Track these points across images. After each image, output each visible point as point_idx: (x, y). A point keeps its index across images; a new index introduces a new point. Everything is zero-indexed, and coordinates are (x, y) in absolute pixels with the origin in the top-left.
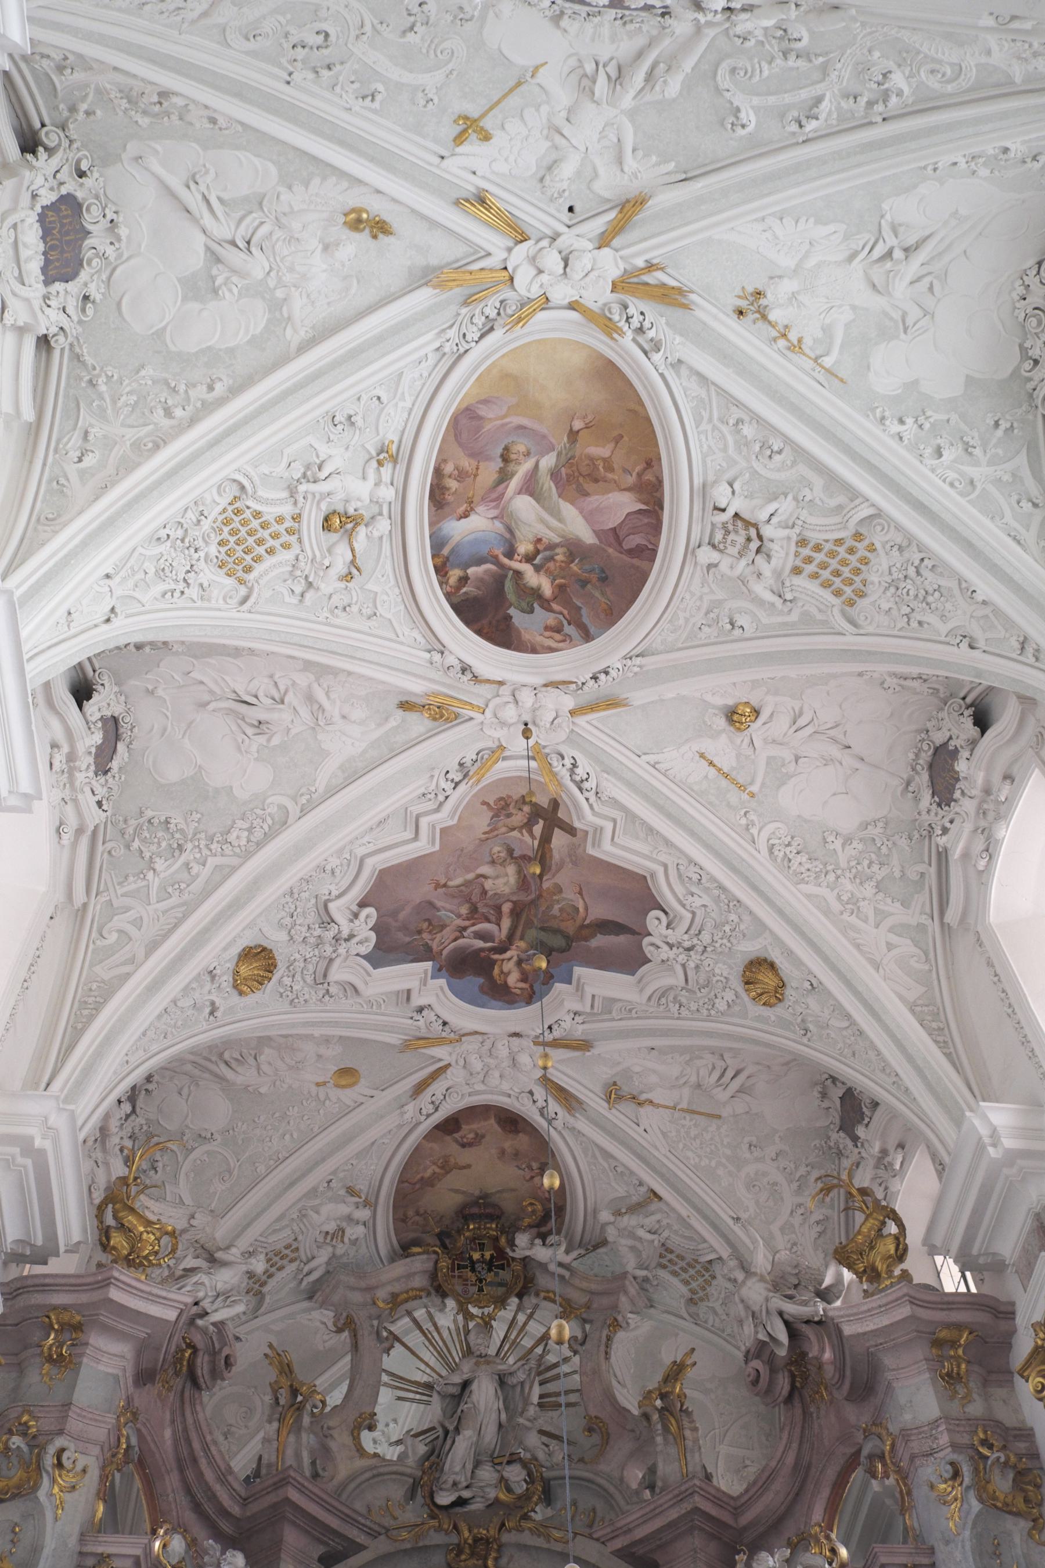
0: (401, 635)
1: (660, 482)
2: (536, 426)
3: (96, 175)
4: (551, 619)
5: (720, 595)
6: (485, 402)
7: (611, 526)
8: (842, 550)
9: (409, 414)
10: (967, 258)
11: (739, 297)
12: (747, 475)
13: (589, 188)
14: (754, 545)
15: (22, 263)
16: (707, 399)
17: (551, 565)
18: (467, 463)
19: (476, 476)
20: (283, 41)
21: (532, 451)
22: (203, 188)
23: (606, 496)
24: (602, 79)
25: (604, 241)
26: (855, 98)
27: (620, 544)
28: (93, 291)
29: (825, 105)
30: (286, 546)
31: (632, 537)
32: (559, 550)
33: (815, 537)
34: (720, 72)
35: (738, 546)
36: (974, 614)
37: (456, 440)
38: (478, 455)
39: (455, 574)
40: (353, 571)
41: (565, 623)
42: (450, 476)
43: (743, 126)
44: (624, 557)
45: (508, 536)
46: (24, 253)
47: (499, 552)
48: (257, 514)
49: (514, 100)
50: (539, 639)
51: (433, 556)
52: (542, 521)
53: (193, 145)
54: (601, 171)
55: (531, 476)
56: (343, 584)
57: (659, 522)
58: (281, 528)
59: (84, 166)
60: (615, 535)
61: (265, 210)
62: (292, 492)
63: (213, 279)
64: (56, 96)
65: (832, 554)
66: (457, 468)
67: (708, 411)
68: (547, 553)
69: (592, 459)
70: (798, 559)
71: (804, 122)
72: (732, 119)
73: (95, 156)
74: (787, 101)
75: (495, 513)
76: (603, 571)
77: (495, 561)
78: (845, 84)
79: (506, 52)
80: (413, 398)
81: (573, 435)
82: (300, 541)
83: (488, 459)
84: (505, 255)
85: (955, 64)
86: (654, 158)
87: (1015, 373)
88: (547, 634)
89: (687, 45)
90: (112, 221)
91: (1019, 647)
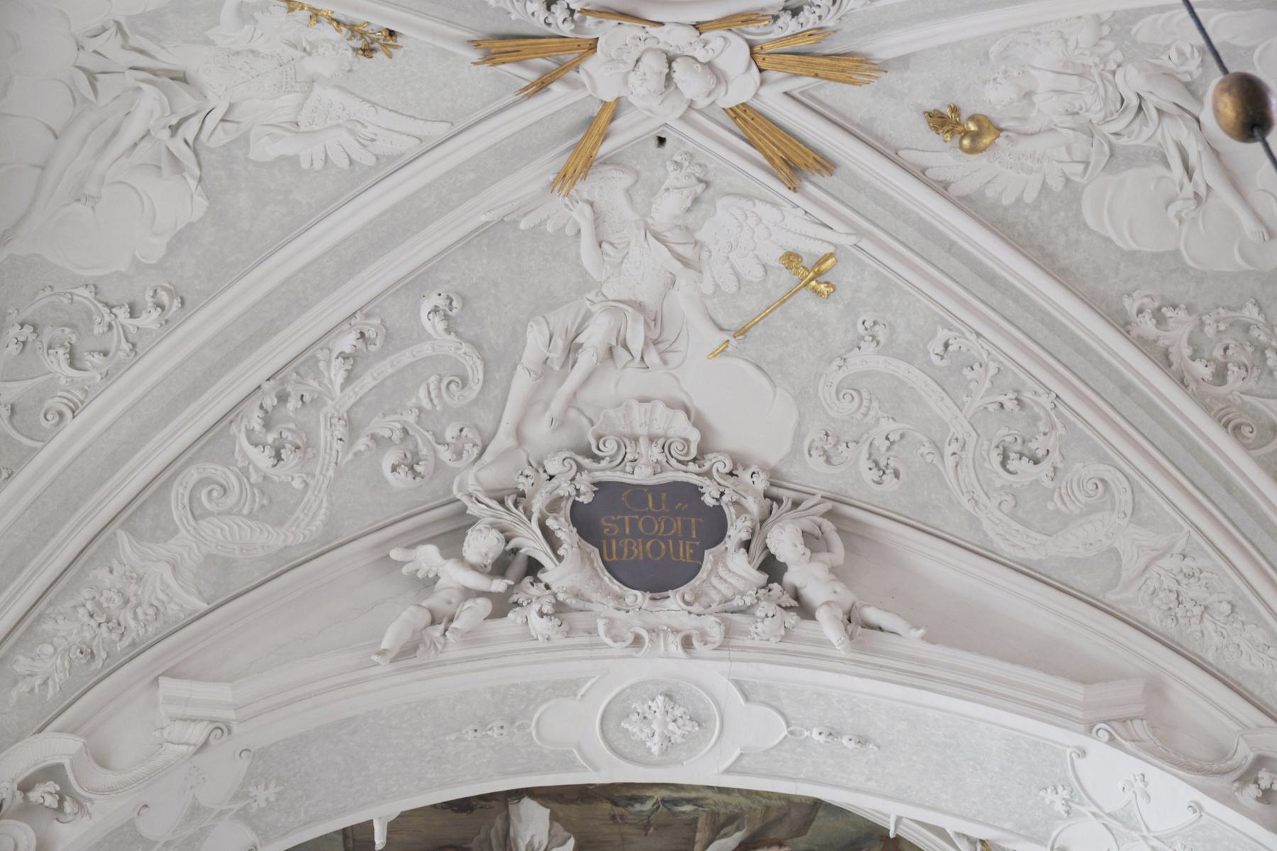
10: (51, 129)
13: (637, 173)
20: (1059, 465)
22: (1189, 188)
25: (614, 110)
29: (339, 378)
34: (481, 376)
43: (436, 310)
53: (1190, 263)
54: (621, 200)
71: (360, 344)
79: (764, 381)
84: (764, 91)
85: (203, 517)
86: (549, 228)
89: (530, 404)
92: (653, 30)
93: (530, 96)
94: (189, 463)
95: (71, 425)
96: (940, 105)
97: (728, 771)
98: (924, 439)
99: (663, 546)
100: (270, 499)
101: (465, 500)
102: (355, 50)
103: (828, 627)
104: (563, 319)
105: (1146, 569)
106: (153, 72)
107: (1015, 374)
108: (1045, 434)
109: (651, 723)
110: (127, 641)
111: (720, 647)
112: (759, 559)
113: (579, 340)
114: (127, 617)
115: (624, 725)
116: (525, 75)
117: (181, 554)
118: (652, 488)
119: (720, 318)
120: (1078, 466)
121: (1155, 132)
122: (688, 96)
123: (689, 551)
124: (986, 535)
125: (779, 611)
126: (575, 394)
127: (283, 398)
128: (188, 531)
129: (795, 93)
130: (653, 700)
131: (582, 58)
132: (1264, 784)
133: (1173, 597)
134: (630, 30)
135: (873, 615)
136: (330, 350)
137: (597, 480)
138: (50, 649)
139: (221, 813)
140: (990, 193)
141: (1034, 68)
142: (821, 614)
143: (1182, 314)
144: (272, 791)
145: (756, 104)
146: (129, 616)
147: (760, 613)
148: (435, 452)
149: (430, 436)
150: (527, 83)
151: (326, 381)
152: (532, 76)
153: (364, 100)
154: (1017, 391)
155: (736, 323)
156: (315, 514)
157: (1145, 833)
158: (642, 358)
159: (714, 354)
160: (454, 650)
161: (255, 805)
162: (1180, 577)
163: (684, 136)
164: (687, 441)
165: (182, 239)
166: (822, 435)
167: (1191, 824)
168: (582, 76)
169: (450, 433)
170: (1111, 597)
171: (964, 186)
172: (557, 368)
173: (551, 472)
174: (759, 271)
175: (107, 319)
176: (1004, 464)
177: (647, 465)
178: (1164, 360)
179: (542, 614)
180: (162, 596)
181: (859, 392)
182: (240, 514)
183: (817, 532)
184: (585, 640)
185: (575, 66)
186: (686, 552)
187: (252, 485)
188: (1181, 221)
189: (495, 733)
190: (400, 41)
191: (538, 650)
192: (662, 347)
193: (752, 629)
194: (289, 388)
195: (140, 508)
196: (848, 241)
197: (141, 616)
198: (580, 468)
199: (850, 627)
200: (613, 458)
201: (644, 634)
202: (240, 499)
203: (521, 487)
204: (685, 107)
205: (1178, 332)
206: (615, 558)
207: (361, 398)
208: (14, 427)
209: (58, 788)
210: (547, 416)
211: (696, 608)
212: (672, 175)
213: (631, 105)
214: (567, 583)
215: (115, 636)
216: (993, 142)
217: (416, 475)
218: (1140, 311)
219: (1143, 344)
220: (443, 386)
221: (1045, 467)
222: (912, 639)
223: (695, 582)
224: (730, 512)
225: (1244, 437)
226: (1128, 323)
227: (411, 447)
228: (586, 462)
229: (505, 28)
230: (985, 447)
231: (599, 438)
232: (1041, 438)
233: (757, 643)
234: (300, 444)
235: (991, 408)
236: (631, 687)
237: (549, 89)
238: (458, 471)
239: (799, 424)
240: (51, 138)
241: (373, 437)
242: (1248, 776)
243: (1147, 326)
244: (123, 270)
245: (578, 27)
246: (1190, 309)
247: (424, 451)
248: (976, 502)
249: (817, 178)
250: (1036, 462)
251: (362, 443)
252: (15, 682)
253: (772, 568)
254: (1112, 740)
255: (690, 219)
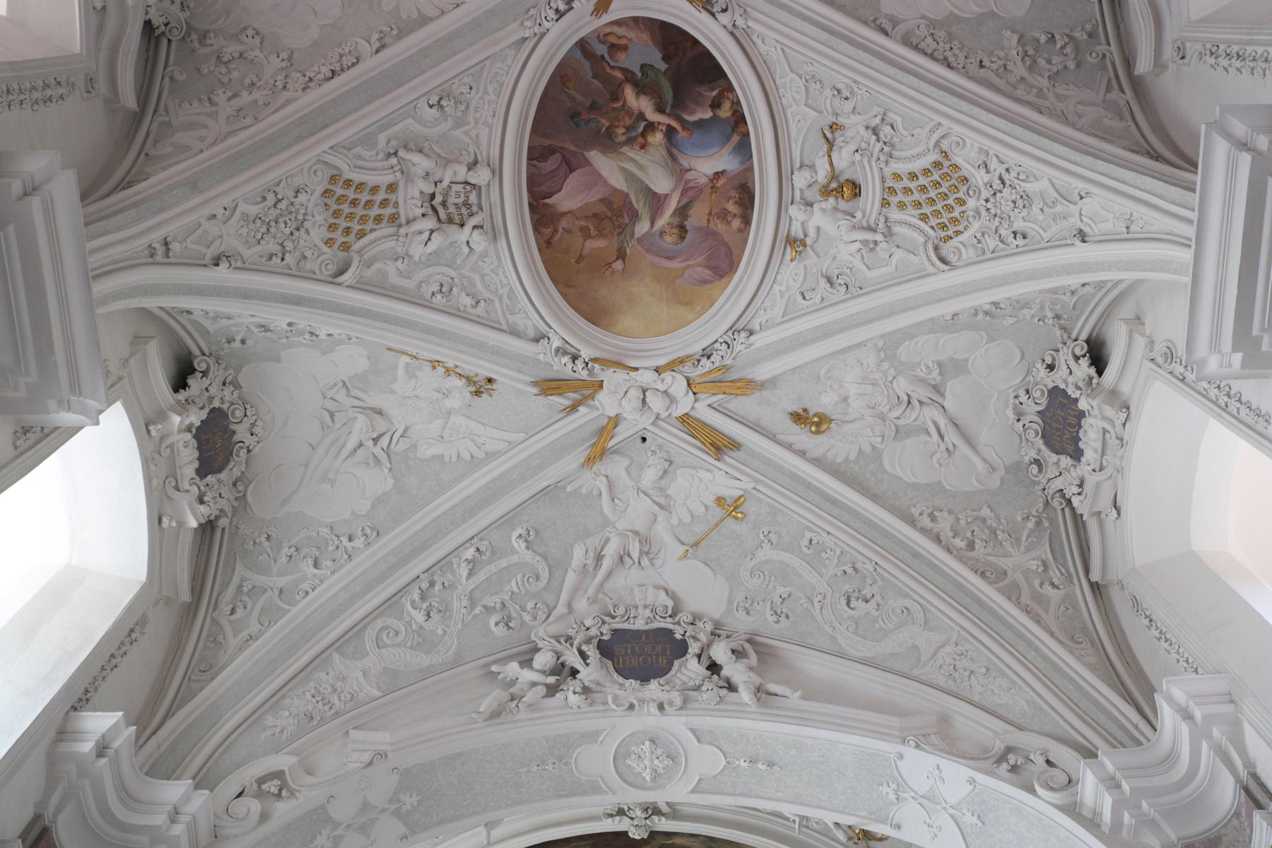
0: (779, 49)
1: (536, 229)
2: (656, 259)
3: (1027, 459)
4: (623, 59)
5: (458, 133)
6: (705, 282)
7: (575, 173)
8: (356, 227)
9: (775, 278)
10: (311, 445)
11: (493, 390)
12: (458, 262)
13: (632, 458)
14: (439, 199)
15: (1101, 439)
16: (507, 314)
17: (628, 122)
18: (719, 226)
19: (710, 214)
20: (881, 602)
21: (657, 238)
22: (943, 447)
23: (584, 202)
24: (635, 554)
25: (616, 421)
26: (444, 587)
27: (564, 156)
28: (1042, 372)
29: (464, 572)
30: (897, 177)
31: (555, 167)
32: (622, 139)
33: (385, 230)
34: (547, 574)
35: (452, 193)
36: (220, 240)
37: (730, 249)
38: (709, 234)
39: (725, 112)
40: (831, 135)
41: (607, 57)
42: (735, 215)
44: (556, 143)
45: (674, 151)
46: (1098, 445)
47: (682, 134)
48: (924, 218)
49: (700, 529)
50: (632, 35)
51: (747, 134)
52: (641, 167)
53: (949, 488)
54: (623, 474)
55: (656, 213)
56: (841, 120)
57: (530, 191)
58: (900, 197)
59: (1035, 469)
60: (571, 164)
61: (893, 428)
62: (889, 234)
63: (941, 373)
64: (1051, 534)
65: (363, 219)
66: (729, 223)
67: (504, 303)
68: (633, 134)
69: (601, 235)
70: (394, 200)
71: (477, 555)
72: (531, 538)
73: (1025, 472)
74: (493, 566)
75: (689, 176)
76: (577, 125)
77: (683, 122)
78: (455, 595)
79: (709, 571)
80: (772, 292)
81: (621, 255)
82: (883, 180)
83: (699, 229)
84: (697, 405)
85: (383, 647)
86: (584, 491)
87: (238, 369)
88: (623, 42)
89: (576, 589)
90: (1018, 420)
91: (171, 247)
92: (633, 374)
93: (569, 414)
94: (377, 617)
95: (312, 595)
96: (796, 408)
97: (693, 791)
98: (802, 596)
99: (650, 659)
100: (424, 639)
101: (536, 640)
102: (471, 392)
103: (745, 695)
104: (594, 542)
105: (935, 654)
106: (363, 408)
107: (852, 554)
108: (871, 585)
109: (644, 760)
110: (333, 711)
111: (681, 709)
112: (706, 663)
113: (603, 553)
114: (335, 699)
115: (628, 762)
116: (563, 402)
117: (369, 667)
118: (647, 632)
119: (682, 538)
120: (892, 601)
121: (919, 414)
122: (655, 411)
123: (665, 661)
124: (841, 646)
125: (715, 688)
126: (602, 584)
127: (432, 584)
128: (374, 655)
129: (715, 405)
130: (643, 744)
131: (595, 391)
132: (1012, 762)
133: (952, 667)
134: (621, 375)
135: (772, 687)
136: (460, 559)
137: (613, 628)
138: (287, 713)
139: (383, 810)
140: (830, 455)
141: (847, 382)
142: (741, 688)
143: (945, 514)
144: (415, 799)
145: (693, 413)
146: (336, 698)
147: (704, 688)
148: (521, 617)
149: (517, 607)
150: (564, 407)
151: (457, 575)
152: (567, 403)
153: (478, 422)
154: (854, 563)
155: (692, 540)
156: (449, 648)
157: (944, 805)
158: (639, 563)
159: (680, 559)
160: (523, 714)
161: (404, 807)
162: (955, 656)
163: (654, 433)
164: (666, 607)
165: (379, 501)
166: (744, 599)
167: (970, 793)
168: (596, 403)
169: (530, 606)
170: (915, 672)
171: (816, 453)
172: (591, 570)
173: (587, 625)
174: (703, 509)
175: (336, 543)
176: (848, 604)
177: (642, 619)
178: (937, 539)
179: (575, 693)
180: (356, 688)
181: (763, 573)
182: (405, 646)
183: (741, 649)
184: (601, 707)
185: (592, 397)
186: (663, 661)
187: (413, 631)
188: (940, 465)
189: (550, 768)
190: (494, 386)
191: (573, 714)
192: (651, 556)
193: (700, 698)
194: (436, 578)
195: (346, 641)
196: (750, 486)
197: (343, 698)
198: (604, 622)
199: (758, 695)
200: (623, 616)
201: (635, 702)
202: (405, 638)
203: (570, 634)
204: (654, 417)
205: (944, 524)
206: (621, 666)
207: (477, 586)
208: (281, 600)
209: (279, 783)
210: (586, 596)
211: (666, 688)
212: (651, 458)
213: (625, 418)
214: (592, 678)
215: (326, 708)
216: (828, 428)
217: (509, 628)
218: (921, 514)
219: (924, 531)
220: (525, 579)
221: (872, 604)
222: (794, 698)
223: (668, 676)
224: (690, 641)
225: (988, 577)
226: (914, 521)
227: (507, 613)
228: (607, 619)
229: (551, 375)
230: (837, 597)
231: (615, 606)
232: (868, 587)
233: (703, 706)
234: (442, 609)
235: (839, 574)
236: (630, 736)
237: (577, 410)
238: (534, 627)
239: (731, 594)
240: (311, 449)
241: (485, 607)
242: (1002, 759)
243: (926, 522)
244: (347, 518)
245: (591, 373)
246: (950, 512)
247: (514, 615)
248: (834, 628)
249: (731, 453)
250: (867, 602)
251: (478, 610)
252: (264, 730)
253: (714, 668)
254: (918, 746)
255: (663, 482)
